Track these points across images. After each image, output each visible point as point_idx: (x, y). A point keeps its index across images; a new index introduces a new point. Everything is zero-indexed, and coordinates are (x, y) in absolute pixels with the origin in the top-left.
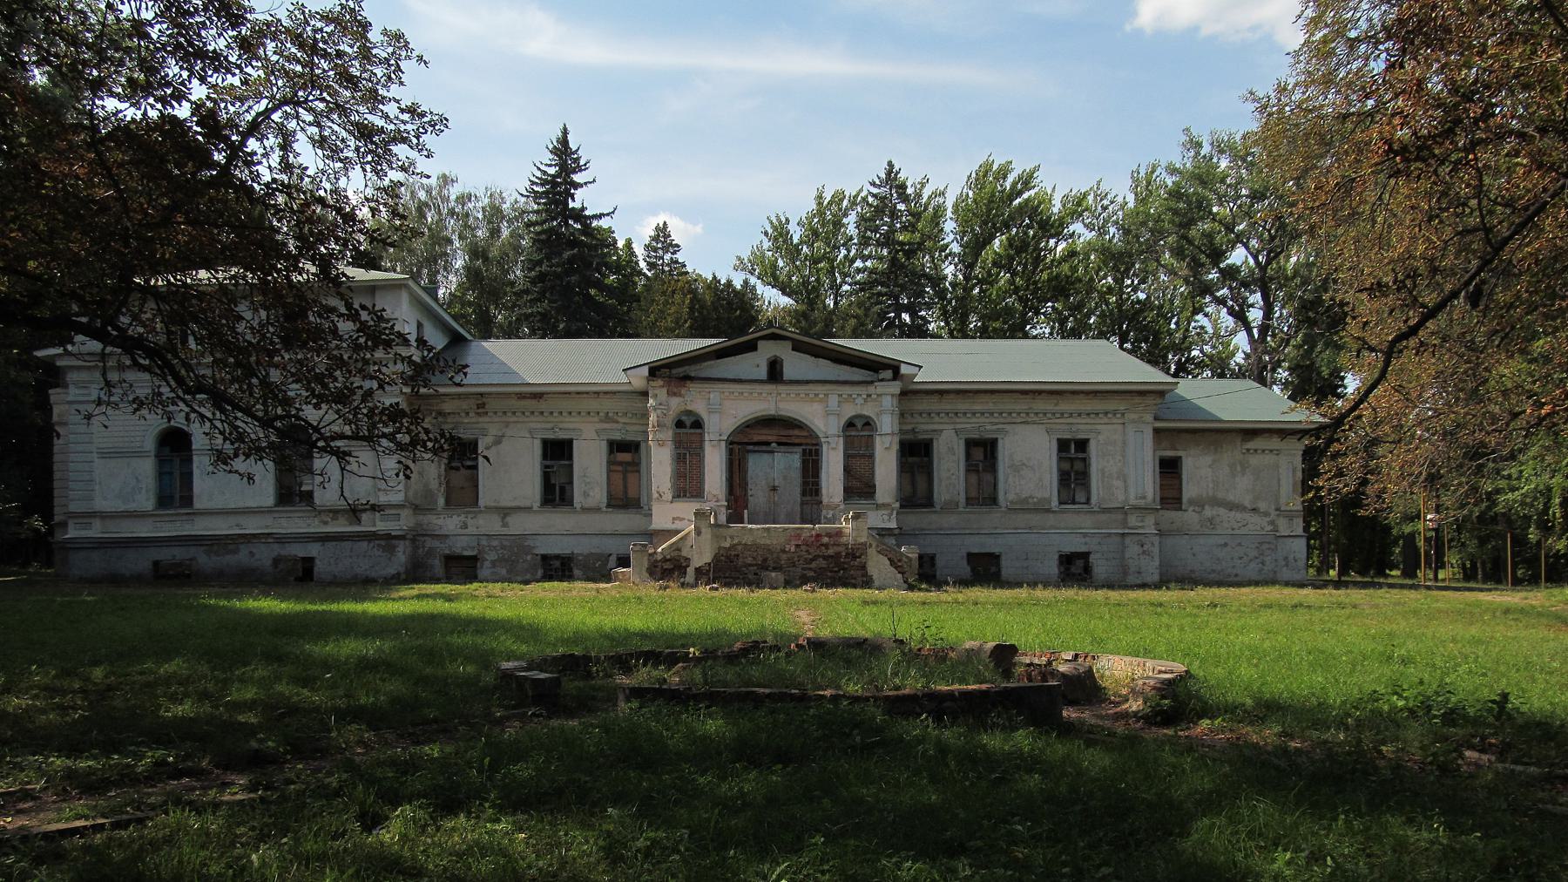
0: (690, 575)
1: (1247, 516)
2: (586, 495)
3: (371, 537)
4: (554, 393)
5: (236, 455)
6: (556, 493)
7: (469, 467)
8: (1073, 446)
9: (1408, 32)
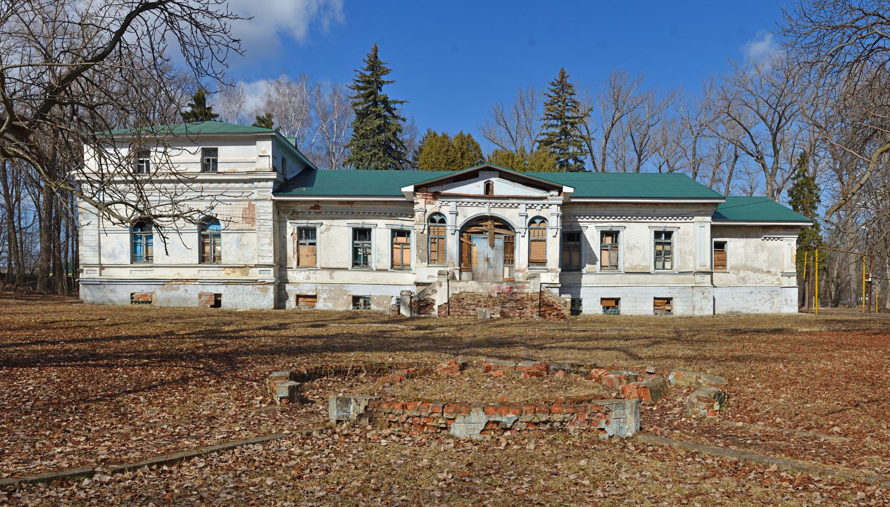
0: (442, 217)
1: (764, 275)
2: (379, 261)
3: (254, 282)
4: (237, 181)
5: (452, 437)
6: (360, 259)
7: (310, 244)
8: (663, 235)
9: (181, 481)
